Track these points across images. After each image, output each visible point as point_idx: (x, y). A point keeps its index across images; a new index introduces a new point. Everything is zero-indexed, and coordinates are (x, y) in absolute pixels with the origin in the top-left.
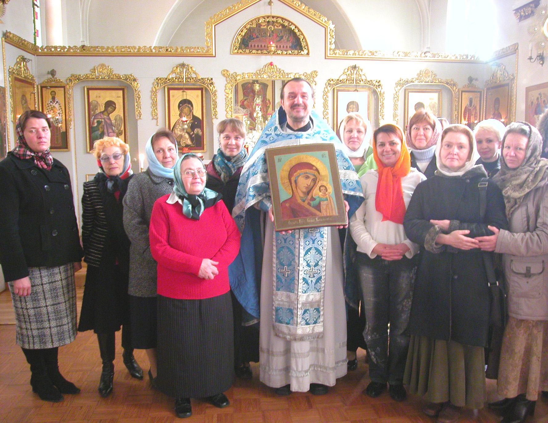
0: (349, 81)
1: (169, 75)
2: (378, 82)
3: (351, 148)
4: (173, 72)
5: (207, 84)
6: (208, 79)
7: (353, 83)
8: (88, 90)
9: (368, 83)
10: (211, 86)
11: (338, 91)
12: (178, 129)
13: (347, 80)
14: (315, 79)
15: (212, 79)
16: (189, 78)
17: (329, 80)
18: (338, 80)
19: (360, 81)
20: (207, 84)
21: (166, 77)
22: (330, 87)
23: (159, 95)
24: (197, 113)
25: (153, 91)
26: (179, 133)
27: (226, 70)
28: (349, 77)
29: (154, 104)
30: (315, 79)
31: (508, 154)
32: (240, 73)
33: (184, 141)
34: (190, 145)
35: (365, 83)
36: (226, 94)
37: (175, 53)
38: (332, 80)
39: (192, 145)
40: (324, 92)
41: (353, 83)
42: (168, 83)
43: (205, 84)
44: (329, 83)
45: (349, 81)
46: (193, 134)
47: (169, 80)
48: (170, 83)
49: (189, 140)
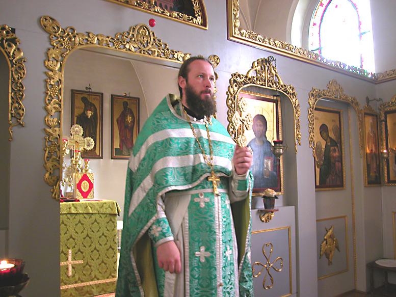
2: (7, 32)
10: (10, 46)
15: (13, 31)
17: (235, 74)
27: (53, 20)
36: (47, 70)
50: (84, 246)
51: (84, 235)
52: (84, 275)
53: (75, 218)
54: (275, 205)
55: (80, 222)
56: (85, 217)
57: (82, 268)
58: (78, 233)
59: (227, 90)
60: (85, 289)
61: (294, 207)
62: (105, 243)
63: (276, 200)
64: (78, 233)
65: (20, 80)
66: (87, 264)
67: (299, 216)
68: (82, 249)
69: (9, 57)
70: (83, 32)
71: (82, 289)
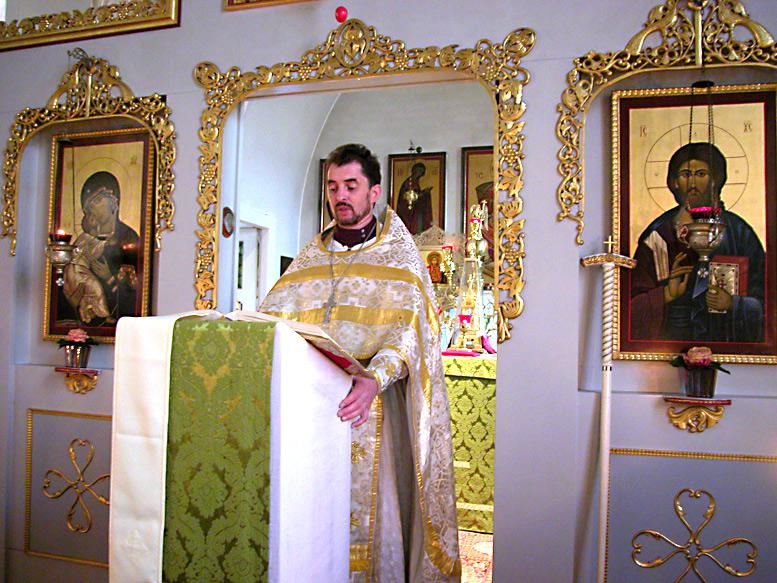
0: (671, 54)
1: (52, 98)
3: (635, 388)
4: (63, 89)
5: (147, 117)
6: (152, 100)
7: (693, 63)
8: (627, 104)
9: (761, 58)
10: (158, 121)
11: (627, 104)
12: (77, 267)
13: (661, 53)
14: (524, 63)
15: (164, 99)
16: (101, 101)
17: (582, 60)
18: (622, 55)
19: (726, 52)
20: (147, 117)
21: (43, 105)
22: (585, 86)
23: (591, 124)
24: (131, 216)
25: (565, 105)
26: (80, 279)
27: (207, 65)
28: (671, 41)
29: (568, 165)
30: (524, 63)
31: (434, 427)
32: (249, 70)
33: (90, 307)
34: (104, 319)
35: (751, 59)
37: (28, 36)
38: (597, 58)
39: (108, 320)
40: (561, 108)
41: (693, 63)
42: (47, 122)
43: (142, 117)
44: (580, 73)
45: (671, 54)
46: (114, 284)
47: (633, 59)
48: (52, 122)
49: (101, 302)
50: (473, 438)
51: (474, 416)
52: (471, 489)
53: (456, 384)
54: (716, 393)
55: (465, 393)
56: (475, 386)
57: (468, 477)
58: (216, 470)
59: (560, 101)
60: (472, 516)
61: (142, 143)
62: (483, 436)
63: (83, 12)
64: (216, 470)
65: (169, 167)
66: (477, 471)
67: (103, 39)
68: (469, 442)
69: (157, 136)
70: (566, 222)
71: (466, 514)
